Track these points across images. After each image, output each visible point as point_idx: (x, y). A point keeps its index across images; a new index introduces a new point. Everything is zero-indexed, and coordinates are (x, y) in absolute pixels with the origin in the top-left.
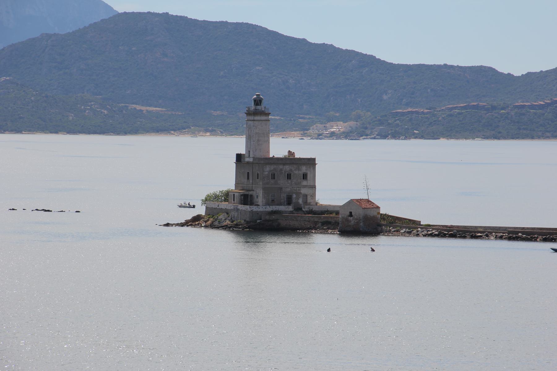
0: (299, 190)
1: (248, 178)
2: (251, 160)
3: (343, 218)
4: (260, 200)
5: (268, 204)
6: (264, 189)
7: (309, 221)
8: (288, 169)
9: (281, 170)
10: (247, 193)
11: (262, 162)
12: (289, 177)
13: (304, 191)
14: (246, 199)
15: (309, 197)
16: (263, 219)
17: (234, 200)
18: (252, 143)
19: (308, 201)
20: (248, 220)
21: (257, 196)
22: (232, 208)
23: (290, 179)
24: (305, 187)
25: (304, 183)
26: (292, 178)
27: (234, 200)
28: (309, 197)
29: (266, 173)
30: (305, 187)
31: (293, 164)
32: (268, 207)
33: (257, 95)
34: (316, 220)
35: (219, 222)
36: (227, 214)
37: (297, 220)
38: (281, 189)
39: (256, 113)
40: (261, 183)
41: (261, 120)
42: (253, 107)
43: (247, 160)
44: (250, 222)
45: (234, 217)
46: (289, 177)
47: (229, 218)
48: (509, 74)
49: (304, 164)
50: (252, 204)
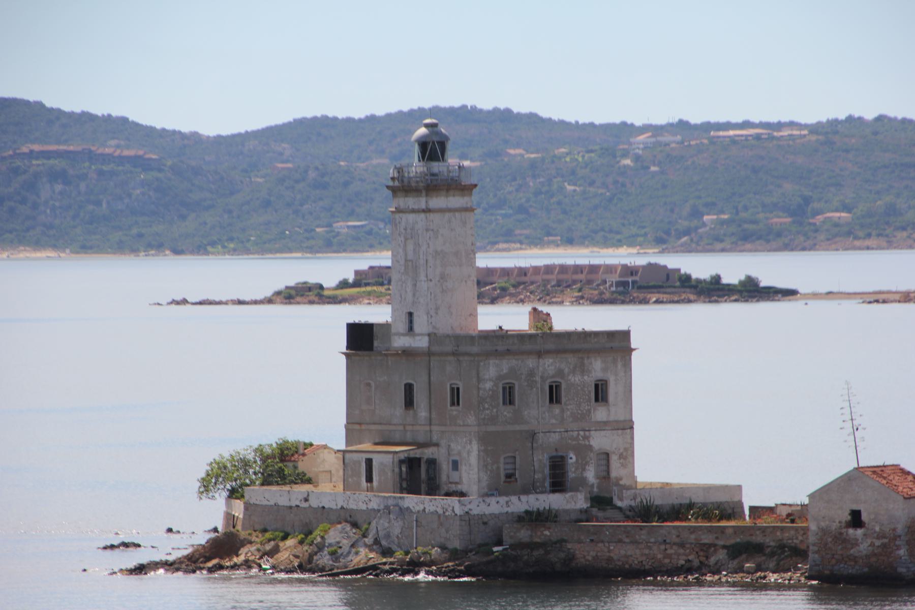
0: (586, 438)
1: (409, 402)
2: (422, 343)
3: (824, 531)
4: (471, 474)
5: (493, 491)
6: (485, 440)
7: (682, 545)
8: (551, 370)
9: (531, 373)
10: (417, 453)
11: (475, 349)
12: (554, 394)
13: (599, 441)
14: (418, 475)
15: (614, 459)
16: (507, 540)
17: (369, 479)
18: (423, 285)
19: (614, 474)
20: (456, 544)
21: (455, 465)
22: (374, 505)
23: (558, 401)
24: (603, 426)
25: (600, 414)
26: (563, 400)
27: (369, 479)
28: (614, 461)
29: (488, 385)
30: (603, 426)
31: (565, 351)
32: (514, 499)
33: (427, 126)
34: (707, 539)
35: (333, 553)
36: (355, 525)
37: (635, 542)
38: (533, 435)
39: (433, 186)
40: (471, 420)
41: (449, 210)
42: (416, 167)
43: (400, 342)
44: (466, 552)
45: (388, 536)
46: (554, 394)
47: (369, 540)
48: (850, 119)
49: (599, 351)
50: (433, 489)
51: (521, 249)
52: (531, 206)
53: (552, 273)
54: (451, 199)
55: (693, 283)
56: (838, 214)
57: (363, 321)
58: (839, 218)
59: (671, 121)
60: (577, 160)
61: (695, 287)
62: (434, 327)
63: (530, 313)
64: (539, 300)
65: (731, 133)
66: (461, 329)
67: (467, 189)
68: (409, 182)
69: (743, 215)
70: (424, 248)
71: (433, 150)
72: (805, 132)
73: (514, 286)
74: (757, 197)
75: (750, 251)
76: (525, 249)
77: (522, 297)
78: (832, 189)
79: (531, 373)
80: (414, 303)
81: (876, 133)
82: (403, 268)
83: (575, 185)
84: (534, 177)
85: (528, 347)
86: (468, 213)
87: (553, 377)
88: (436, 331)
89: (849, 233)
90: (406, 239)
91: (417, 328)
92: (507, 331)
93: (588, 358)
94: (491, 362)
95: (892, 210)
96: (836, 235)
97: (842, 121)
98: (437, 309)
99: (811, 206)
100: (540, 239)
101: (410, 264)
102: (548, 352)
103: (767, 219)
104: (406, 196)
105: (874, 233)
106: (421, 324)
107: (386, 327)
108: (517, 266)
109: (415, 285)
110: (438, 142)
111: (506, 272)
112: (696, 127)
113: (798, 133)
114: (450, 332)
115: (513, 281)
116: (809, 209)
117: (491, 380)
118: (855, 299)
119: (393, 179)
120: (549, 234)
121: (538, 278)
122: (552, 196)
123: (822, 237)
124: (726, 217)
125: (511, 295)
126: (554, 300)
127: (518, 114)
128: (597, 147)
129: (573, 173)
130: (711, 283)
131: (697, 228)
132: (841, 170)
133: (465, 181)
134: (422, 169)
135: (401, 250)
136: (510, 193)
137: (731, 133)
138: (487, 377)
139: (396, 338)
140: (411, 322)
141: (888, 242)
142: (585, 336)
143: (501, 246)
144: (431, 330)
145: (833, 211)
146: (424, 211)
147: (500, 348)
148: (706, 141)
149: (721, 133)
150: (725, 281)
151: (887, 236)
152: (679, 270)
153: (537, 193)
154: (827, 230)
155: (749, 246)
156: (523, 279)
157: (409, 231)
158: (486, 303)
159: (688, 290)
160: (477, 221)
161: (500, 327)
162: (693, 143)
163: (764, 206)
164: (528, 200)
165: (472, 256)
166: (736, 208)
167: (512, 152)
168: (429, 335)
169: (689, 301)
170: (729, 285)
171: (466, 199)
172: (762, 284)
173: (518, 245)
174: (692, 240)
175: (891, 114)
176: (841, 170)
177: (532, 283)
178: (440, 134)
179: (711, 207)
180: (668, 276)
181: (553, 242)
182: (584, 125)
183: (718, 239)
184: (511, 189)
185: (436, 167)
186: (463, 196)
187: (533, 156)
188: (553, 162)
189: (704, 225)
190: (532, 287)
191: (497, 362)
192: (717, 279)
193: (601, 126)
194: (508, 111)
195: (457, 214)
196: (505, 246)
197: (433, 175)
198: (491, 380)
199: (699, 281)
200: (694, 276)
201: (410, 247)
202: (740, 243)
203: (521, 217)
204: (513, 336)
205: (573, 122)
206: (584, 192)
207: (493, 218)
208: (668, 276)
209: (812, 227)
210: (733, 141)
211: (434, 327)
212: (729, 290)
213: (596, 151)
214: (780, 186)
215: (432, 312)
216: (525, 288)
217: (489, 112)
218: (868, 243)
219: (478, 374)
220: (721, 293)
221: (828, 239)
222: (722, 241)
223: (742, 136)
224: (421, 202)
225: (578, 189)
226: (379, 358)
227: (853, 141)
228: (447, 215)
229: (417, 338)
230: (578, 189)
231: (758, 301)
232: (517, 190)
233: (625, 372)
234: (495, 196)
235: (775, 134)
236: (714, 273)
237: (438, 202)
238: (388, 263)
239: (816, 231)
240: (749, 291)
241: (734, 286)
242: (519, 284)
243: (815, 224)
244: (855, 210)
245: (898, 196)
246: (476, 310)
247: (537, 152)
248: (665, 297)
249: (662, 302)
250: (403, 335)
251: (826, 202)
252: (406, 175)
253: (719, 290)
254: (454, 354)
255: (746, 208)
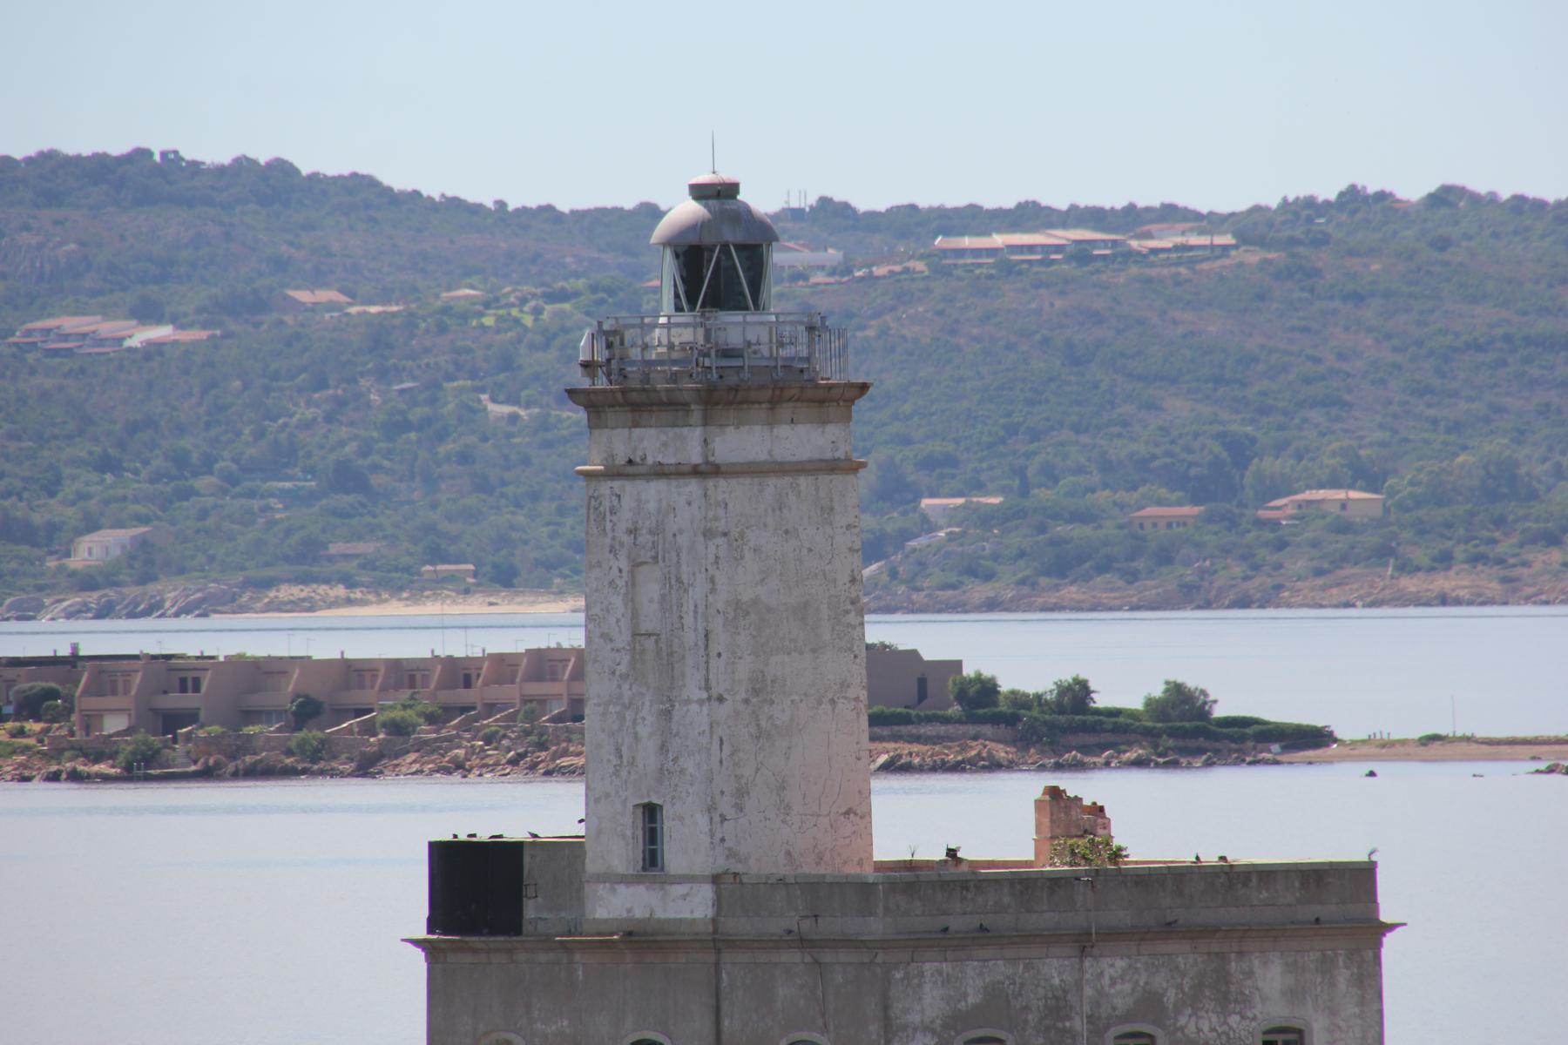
2: (691, 906)
8: (1121, 996)
9: (1058, 1007)
11: (876, 927)
18: (695, 716)
31: (1168, 930)
39: (725, 389)
42: (667, 328)
43: (615, 905)
48: (1352, 198)
49: (1272, 934)
51: (349, 602)
52: (375, 468)
53: (554, 677)
54: (783, 431)
55: (1003, 707)
56: (1340, 495)
57: (483, 836)
58: (1344, 506)
59: (794, 204)
60: (517, 321)
61: (1011, 720)
62: (732, 854)
63: (1039, 804)
64: (513, 762)
65: (998, 240)
66: (820, 859)
67: (838, 400)
68: (646, 378)
69: (1043, 495)
70: (697, 592)
71: (725, 274)
72: (1228, 239)
73: (431, 719)
74: (1085, 439)
75: (1078, 608)
76: (363, 603)
77: (461, 752)
78: (1316, 415)
79: (1058, 1007)
80: (662, 774)
81: (1443, 244)
82: (626, 659)
83: (512, 400)
84: (383, 375)
85: (1044, 918)
86: (837, 480)
87: (1128, 1017)
88: (739, 868)
89: (1383, 553)
90: (636, 565)
91: (674, 859)
92: (975, 865)
93: (1241, 953)
94: (928, 968)
95: (1503, 484)
96: (1343, 559)
97: (1327, 203)
98: (741, 793)
99: (1252, 468)
100: (407, 569)
101: (650, 644)
102: (1113, 935)
103: (1122, 506)
104: (636, 425)
105: (1460, 552)
106: (687, 847)
107: (566, 852)
108: (442, 652)
109: (667, 714)
110: (740, 248)
111: (404, 674)
112: (872, 221)
113: (1204, 240)
114: (784, 870)
115: (426, 704)
116: (1248, 479)
117: (927, 1028)
118: (1513, 759)
119: (587, 366)
120: (437, 555)
121: (509, 693)
122: (441, 436)
123: (1298, 564)
124: (995, 500)
125: (421, 746)
126: (564, 762)
127: (314, 177)
128: (580, 284)
129: (507, 363)
130: (1059, 707)
131: (904, 536)
132: (1342, 357)
133: (831, 373)
134: (687, 335)
135: (618, 601)
136: (307, 425)
137: (998, 240)
138: (915, 1018)
139: (602, 890)
140: (652, 836)
141: (1505, 580)
142: (1229, 879)
143: (287, 592)
144: (721, 864)
145: (1321, 486)
146: (696, 472)
147: (956, 923)
148: (920, 266)
149: (967, 242)
150: (1101, 701)
151: (1501, 561)
152: (957, 665)
153: (396, 426)
154: (1315, 544)
155: (1071, 592)
156: (462, 696)
157: (645, 538)
158: (342, 775)
159: (987, 729)
160: (203, 514)
161: (952, 853)
162: (879, 271)
163: (1107, 466)
164: (365, 451)
165: (852, 618)
166: (1020, 472)
167: (304, 296)
168: (716, 879)
169: (994, 766)
170: (1116, 713)
171: (832, 431)
172: (1219, 712)
173: (340, 591)
174: (893, 574)
175: (1480, 185)
176: (1342, 357)
177: (491, 708)
178: (745, 217)
179: (941, 469)
180: (922, 682)
181: (450, 578)
182: (523, 211)
183: (976, 571)
184: (311, 412)
185: (734, 326)
186: (824, 422)
187: (373, 309)
188: (442, 329)
189: (927, 525)
190: (490, 723)
191: (946, 967)
192: (1077, 694)
193: (578, 215)
194: (282, 168)
195: (804, 481)
196: (297, 592)
197: (727, 353)
198: (927, 1028)
199: (1020, 701)
200: (1005, 686)
201: (650, 589)
202: (1044, 581)
203: (344, 500)
204: (997, 881)
205: (490, 204)
206: (543, 425)
207: (256, 504)
208: (922, 682)
209: (1269, 535)
210: (1006, 265)
211: (732, 854)
212: (1118, 729)
213: (576, 294)
214: (1153, 406)
215: (725, 805)
216: (465, 727)
217: (220, 171)
218: (1442, 582)
219: (886, 1007)
220: (1091, 739)
221: (1319, 573)
222: (989, 576)
223: (1031, 248)
224: (689, 444)
225: (522, 413)
226: (543, 957)
227: (1376, 267)
228: (773, 483)
229: (677, 890)
230: (522, 413)
231: (1209, 764)
232: (329, 418)
233: (1362, 1002)
234: (259, 434)
235: (1134, 244)
236: (1067, 677)
237: (741, 441)
238: (575, 638)
239: (1281, 545)
240: (1174, 733)
241: (1132, 714)
242: (450, 711)
243: (1274, 525)
244: (1391, 481)
245: (1520, 436)
246: (865, 795)
247: (385, 297)
248: (915, 752)
249: (907, 769)
250: (625, 880)
251: (1299, 457)
252: (635, 353)
253: (1085, 728)
254: (803, 942)
255: (1051, 475)
